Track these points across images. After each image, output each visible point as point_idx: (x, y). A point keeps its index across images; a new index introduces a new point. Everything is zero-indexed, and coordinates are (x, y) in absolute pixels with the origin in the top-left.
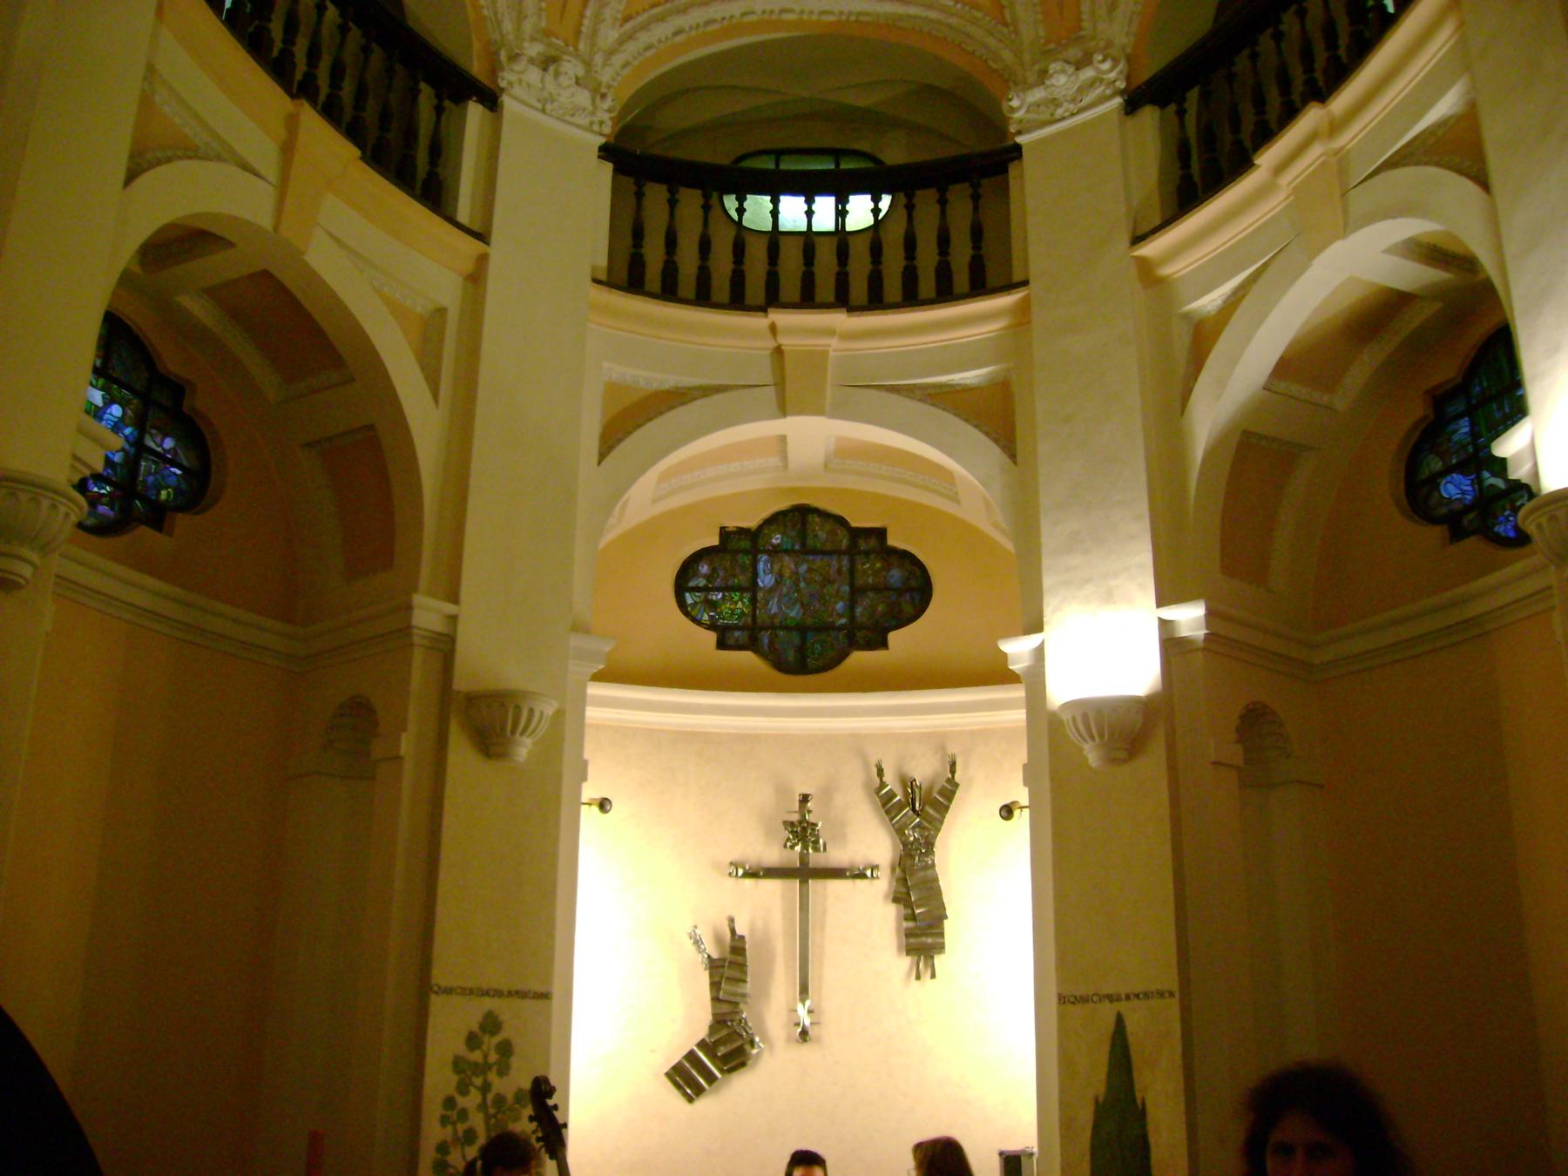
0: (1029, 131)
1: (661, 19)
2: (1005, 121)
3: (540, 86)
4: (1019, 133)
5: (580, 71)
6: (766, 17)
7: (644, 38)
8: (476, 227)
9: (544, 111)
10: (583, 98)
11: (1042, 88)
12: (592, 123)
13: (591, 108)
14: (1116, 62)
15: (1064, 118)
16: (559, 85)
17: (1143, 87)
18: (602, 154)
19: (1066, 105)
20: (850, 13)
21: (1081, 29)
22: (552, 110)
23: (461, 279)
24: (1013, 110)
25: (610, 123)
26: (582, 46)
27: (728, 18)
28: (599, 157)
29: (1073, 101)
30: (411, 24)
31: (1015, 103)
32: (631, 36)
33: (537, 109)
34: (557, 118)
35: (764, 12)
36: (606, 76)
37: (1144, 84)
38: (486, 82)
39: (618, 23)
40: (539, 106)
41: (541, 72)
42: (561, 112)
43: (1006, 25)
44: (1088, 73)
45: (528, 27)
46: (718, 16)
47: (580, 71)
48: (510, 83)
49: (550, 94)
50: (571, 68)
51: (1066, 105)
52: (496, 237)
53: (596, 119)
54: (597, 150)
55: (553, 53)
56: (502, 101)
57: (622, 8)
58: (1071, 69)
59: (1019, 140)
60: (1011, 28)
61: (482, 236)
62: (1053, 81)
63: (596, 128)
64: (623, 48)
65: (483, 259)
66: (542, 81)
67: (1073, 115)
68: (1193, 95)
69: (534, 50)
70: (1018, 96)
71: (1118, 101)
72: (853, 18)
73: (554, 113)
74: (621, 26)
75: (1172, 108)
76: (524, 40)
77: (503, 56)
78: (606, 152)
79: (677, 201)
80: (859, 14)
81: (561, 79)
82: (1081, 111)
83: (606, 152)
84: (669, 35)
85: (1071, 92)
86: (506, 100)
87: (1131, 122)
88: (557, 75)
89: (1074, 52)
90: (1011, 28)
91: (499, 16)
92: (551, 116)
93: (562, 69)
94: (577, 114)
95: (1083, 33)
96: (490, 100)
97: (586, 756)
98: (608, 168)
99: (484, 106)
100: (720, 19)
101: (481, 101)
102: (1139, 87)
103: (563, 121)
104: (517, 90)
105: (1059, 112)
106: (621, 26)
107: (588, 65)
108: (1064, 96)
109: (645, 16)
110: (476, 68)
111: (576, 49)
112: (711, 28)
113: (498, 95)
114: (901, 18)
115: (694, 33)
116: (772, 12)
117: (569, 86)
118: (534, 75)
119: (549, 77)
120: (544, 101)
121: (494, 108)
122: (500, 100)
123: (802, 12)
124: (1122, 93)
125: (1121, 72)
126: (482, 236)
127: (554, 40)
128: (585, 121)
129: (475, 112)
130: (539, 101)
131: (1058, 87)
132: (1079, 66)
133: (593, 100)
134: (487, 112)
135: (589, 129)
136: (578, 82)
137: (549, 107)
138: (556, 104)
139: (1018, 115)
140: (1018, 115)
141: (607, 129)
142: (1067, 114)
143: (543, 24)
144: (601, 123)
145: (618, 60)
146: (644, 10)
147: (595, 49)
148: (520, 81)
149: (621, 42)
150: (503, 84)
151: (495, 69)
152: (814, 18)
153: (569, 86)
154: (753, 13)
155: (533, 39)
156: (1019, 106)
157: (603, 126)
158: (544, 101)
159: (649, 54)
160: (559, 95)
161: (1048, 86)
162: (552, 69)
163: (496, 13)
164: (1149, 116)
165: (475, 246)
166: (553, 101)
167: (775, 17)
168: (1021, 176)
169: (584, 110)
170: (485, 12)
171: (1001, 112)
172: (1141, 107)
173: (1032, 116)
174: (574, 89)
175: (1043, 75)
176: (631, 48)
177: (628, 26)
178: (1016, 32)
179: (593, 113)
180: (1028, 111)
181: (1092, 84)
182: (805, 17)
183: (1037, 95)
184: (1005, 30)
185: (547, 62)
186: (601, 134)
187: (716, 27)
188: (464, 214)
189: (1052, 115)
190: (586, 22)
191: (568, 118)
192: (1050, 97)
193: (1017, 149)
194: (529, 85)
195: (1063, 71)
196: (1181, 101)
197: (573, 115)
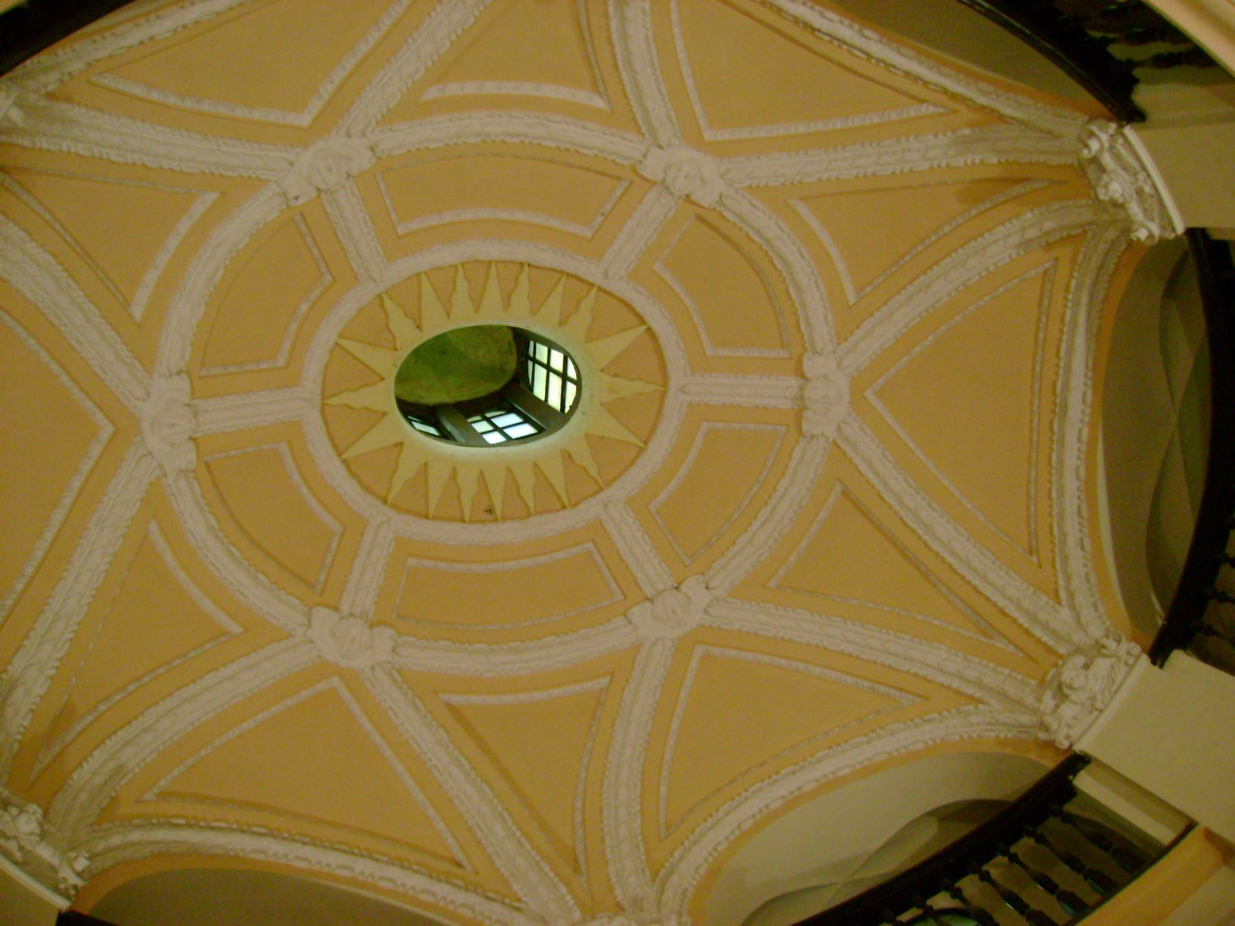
0: (1170, 221)
1: (1065, 561)
2: (1163, 242)
3: (1079, 706)
4: (1174, 230)
5: (1080, 660)
6: (1083, 456)
7: (1076, 583)
8: (1181, 826)
9: (1101, 711)
10: (1101, 665)
11: (1127, 206)
12: (1126, 663)
13: (1114, 660)
14: (1092, 135)
15: (1154, 186)
16: (1082, 688)
17: (1109, 106)
18: (1158, 663)
19: (1140, 183)
20: (1086, 376)
21: (1072, 165)
22: (1103, 702)
23: (1224, 869)
24: (1151, 236)
25: (1133, 644)
26: (1062, 650)
27: (1079, 493)
28: (1161, 666)
29: (1135, 174)
30: (1013, 799)
31: (1142, 235)
32: (1071, 597)
33: (1097, 718)
34: (1112, 698)
35: (1079, 458)
36: (1096, 631)
37: (1106, 106)
38: (1060, 759)
39: (1057, 606)
40: (1095, 713)
41: (1067, 702)
42: (1107, 693)
43: (1085, 232)
44: (1107, 160)
45: (1030, 700)
46: (1076, 502)
47: (1080, 660)
48: (1067, 737)
49: (1089, 698)
50: (1071, 672)
51: (1140, 183)
52: (1194, 815)
53: (1125, 656)
54: (1152, 666)
55: (1055, 684)
56: (1080, 751)
57: (1045, 598)
58: (1105, 178)
59: (1180, 229)
60: (1087, 228)
61: (1191, 826)
62: (1117, 196)
63: (1131, 661)
64: (1078, 608)
65: (1209, 835)
66: (1076, 703)
67: (1149, 176)
68: (1119, 51)
69: (1048, 701)
70: (1136, 230)
71: (1128, 131)
72: (1090, 374)
73: (1105, 701)
74: (1059, 603)
75: (1137, 72)
76: (1038, 708)
77: (1042, 736)
78: (1158, 654)
79: (1223, 593)
80: (1087, 368)
81: (1076, 685)
82: (1144, 168)
83: (1158, 654)
84: (1082, 554)
85: (1128, 178)
86: (1078, 748)
87: (1154, 115)
88: (1071, 687)
89: (1091, 172)
90: (1087, 228)
91: (1017, 724)
92: (1106, 707)
93: (1068, 681)
94: (1113, 675)
95: (1076, 163)
96: (1077, 762)
97: (957, 900)
98: (1180, 659)
99: (1080, 770)
100: (1079, 502)
101: (1075, 772)
102: (1110, 110)
103: (1115, 692)
104: (1074, 733)
105: (1147, 189)
106: (1059, 603)
107: (1078, 650)
108: (1132, 184)
109: (1060, 575)
110: (1050, 763)
111: (1061, 657)
112: (1085, 513)
113: (1073, 753)
114: (1088, 329)
115: (1086, 530)
116: (1079, 450)
117: (1086, 677)
118: (1068, 710)
119: (1073, 696)
120: (1093, 708)
121: (1087, 759)
122: (1078, 752)
123: (1082, 421)
124: (1121, 126)
125: (1101, 129)
126: (1191, 826)
127: (1049, 677)
128: (1123, 669)
129: (1084, 782)
130: (1091, 712)
131: (1124, 191)
132: (1102, 169)
133: (1105, 656)
134: (1088, 767)
135: (1131, 668)
136: (1086, 667)
137: (1098, 705)
138: (1099, 697)
139: (1156, 231)
140: (1156, 231)
141: (1136, 649)
142: (1149, 182)
143: (1034, 683)
144: (1129, 653)
145: (1087, 615)
146: (1055, 575)
147: (1067, 638)
148: (1069, 726)
149: (1072, 607)
150: (1065, 745)
151: (1050, 745)
152: (1088, 411)
153: (1086, 677)
154: (1077, 468)
155: (1039, 700)
156: (1146, 230)
157: (1132, 652)
158: (1093, 708)
159: (1093, 580)
160: (1091, 690)
161: (1125, 200)
162: (1066, 691)
163: (1015, 726)
164: (1143, 96)
165: (1194, 837)
166: (1094, 699)
167: (1084, 448)
168: (1218, 229)
169: (1112, 667)
170: (1010, 735)
171: (1152, 248)
172: (1136, 107)
173: (1156, 215)
174: (1090, 673)
175: (1115, 204)
176: (1079, 599)
177: (1063, 595)
178: (1089, 224)
179: (1119, 659)
180: (1152, 220)
181: (1117, 157)
182: (1087, 419)
183: (1135, 209)
184: (1090, 234)
185: (1061, 694)
186: (1138, 657)
187: (1084, 507)
188: (1162, 833)
189: (1152, 196)
190: (1045, 639)
191: (1114, 689)
192: (1135, 196)
193: (1190, 232)
194: (1075, 718)
195: (1106, 186)
196: (1131, 64)
197: (1114, 682)
